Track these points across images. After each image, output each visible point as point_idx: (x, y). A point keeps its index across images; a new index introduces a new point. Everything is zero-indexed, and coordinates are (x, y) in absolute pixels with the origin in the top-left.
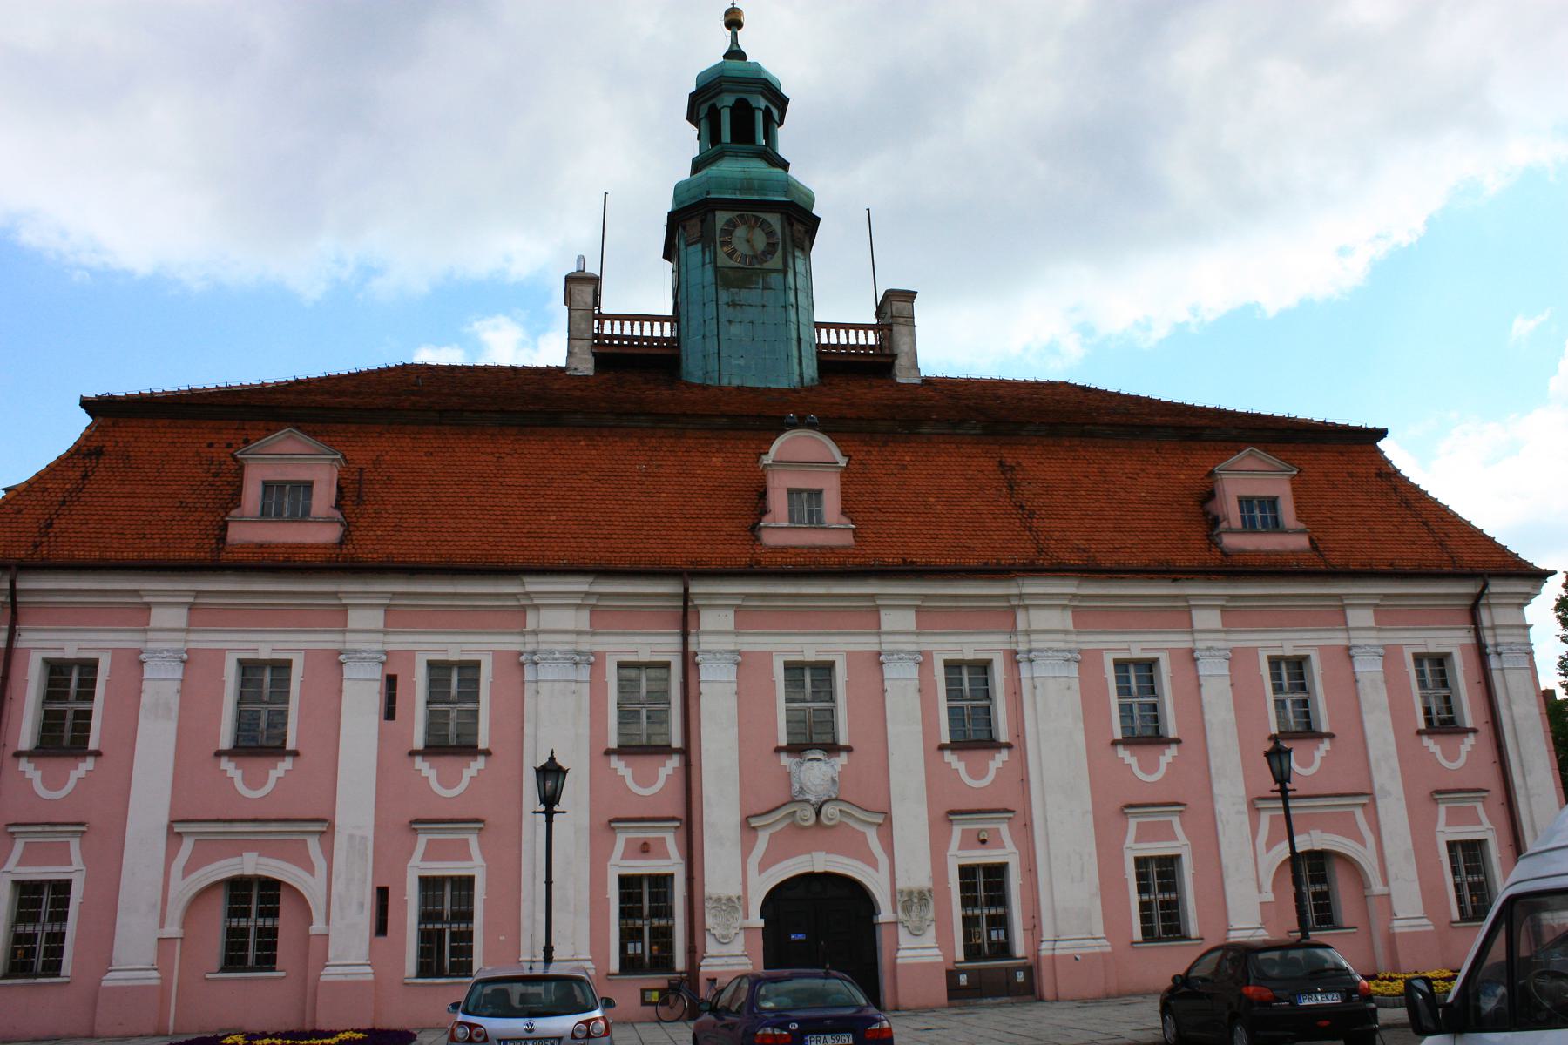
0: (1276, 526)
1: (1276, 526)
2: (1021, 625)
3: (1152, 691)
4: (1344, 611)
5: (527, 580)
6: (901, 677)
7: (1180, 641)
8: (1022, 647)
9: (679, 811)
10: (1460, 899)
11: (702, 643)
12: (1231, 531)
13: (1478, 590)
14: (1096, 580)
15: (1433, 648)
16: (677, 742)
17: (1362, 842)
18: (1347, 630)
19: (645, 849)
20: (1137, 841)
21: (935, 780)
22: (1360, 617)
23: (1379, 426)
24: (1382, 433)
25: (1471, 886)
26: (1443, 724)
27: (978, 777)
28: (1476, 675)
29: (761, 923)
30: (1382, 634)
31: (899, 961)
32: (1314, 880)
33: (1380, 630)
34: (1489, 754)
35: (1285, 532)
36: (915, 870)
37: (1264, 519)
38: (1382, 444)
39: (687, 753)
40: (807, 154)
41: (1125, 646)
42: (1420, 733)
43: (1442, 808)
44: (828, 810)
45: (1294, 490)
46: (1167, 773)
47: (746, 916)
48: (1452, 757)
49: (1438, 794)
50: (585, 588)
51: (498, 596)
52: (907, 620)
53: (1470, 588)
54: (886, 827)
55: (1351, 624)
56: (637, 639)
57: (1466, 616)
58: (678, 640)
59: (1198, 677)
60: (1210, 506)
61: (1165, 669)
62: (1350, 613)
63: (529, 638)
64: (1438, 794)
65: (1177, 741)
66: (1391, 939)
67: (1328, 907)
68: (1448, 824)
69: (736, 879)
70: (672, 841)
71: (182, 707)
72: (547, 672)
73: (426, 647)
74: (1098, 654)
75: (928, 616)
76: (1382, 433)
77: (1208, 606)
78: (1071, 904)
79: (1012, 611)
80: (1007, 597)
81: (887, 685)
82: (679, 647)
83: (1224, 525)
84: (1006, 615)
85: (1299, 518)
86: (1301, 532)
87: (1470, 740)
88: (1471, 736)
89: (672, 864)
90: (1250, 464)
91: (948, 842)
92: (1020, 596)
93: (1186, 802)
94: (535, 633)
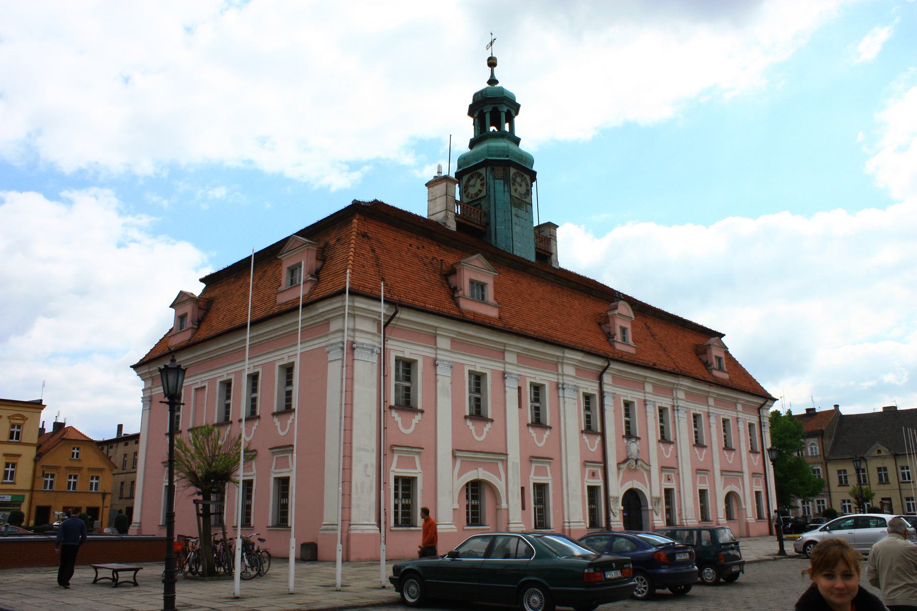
0: (482, 299)
1: (482, 299)
2: (560, 371)
4: (436, 337)
5: (566, 351)
7: (499, 367)
8: (561, 381)
10: (396, 514)
11: (606, 388)
13: (392, 314)
15: (407, 355)
16: (599, 430)
17: (500, 478)
18: (436, 349)
19: (593, 474)
20: (397, 467)
21: (524, 442)
25: (404, 506)
27: (541, 440)
29: (622, 508)
30: (453, 355)
31: (439, 531)
32: (406, 496)
33: (452, 352)
35: (487, 304)
40: (530, 132)
41: (402, 349)
43: (534, 465)
44: (639, 463)
45: (495, 283)
46: (414, 431)
48: (480, 434)
49: (533, 459)
50: (580, 358)
51: (663, 381)
53: (600, 363)
54: (649, 472)
55: (439, 345)
56: (588, 383)
58: (597, 385)
59: (436, 375)
60: (452, 280)
62: (439, 339)
64: (533, 459)
65: (422, 412)
68: (535, 475)
70: (600, 473)
71: (452, 389)
73: (398, 348)
76: (724, 335)
78: (355, 502)
79: (556, 364)
81: (507, 389)
83: (461, 293)
84: (554, 366)
85: (495, 299)
86: (495, 306)
88: (420, 415)
90: (477, 264)
92: (677, 384)
93: (422, 449)
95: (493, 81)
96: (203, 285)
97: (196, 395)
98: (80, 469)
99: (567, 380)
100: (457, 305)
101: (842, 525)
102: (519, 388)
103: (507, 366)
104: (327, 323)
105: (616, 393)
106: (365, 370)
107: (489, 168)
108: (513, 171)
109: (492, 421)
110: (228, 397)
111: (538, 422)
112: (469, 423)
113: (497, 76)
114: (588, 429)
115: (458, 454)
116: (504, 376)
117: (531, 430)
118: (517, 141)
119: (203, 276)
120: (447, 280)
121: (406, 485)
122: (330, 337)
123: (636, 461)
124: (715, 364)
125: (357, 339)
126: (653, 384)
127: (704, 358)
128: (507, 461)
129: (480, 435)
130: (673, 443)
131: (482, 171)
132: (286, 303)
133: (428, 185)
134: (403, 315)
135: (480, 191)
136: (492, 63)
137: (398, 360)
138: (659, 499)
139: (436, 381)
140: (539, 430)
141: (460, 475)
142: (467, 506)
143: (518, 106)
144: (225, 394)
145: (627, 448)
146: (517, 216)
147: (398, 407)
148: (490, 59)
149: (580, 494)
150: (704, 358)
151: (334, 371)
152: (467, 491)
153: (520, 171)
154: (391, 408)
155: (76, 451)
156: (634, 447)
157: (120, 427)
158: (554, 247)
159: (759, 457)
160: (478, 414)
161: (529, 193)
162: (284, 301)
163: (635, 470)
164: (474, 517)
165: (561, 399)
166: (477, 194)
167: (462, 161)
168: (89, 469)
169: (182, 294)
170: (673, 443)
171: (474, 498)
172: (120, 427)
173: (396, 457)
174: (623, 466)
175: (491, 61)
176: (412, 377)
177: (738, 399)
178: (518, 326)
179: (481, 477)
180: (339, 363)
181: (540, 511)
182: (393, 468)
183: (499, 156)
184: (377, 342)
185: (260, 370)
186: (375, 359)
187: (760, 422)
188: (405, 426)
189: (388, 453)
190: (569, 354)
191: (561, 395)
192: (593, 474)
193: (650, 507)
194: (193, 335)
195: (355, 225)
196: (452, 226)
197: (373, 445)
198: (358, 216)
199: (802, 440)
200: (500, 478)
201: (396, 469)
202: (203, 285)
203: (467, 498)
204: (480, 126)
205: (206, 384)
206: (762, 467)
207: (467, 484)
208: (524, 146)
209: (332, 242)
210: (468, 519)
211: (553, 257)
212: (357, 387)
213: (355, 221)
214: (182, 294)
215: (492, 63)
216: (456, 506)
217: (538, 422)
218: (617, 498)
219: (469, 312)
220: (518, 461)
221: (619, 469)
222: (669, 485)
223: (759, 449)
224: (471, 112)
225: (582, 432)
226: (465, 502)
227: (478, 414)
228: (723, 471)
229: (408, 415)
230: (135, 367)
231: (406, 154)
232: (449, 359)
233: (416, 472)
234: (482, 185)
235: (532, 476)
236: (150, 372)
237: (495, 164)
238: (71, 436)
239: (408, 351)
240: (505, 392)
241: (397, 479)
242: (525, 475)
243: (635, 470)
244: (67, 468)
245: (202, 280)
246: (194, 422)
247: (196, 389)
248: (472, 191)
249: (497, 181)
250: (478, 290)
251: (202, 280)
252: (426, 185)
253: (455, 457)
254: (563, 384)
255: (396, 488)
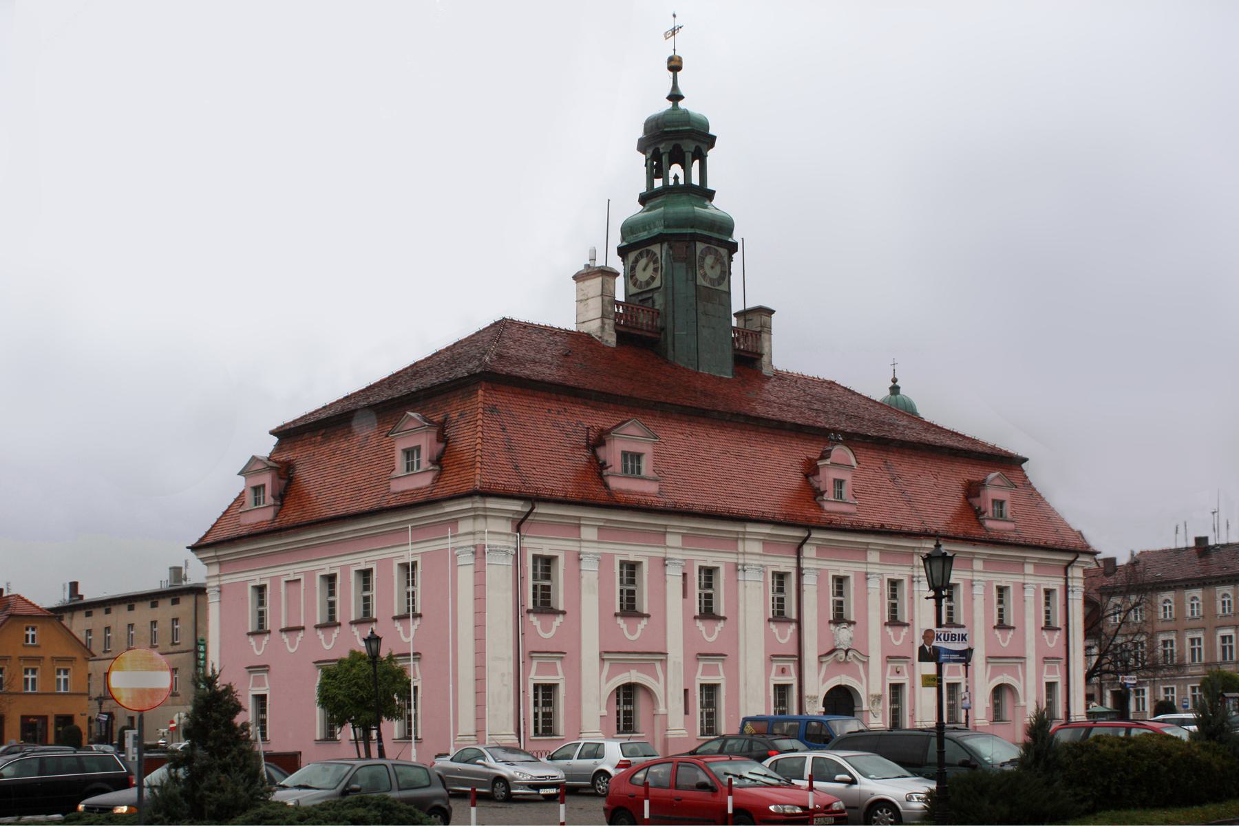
2: (741, 550)
3: (548, 577)
6: (589, 569)
7: (572, 546)
9: (793, 651)
10: (536, 723)
11: (806, 564)
12: (614, 475)
13: (527, 510)
14: (626, 513)
16: (794, 616)
19: (783, 671)
20: (537, 674)
21: (689, 637)
22: (589, 533)
23: (1025, 456)
24: (1025, 460)
25: (544, 714)
26: (1048, 627)
27: (710, 634)
28: (1063, 602)
30: (601, 546)
34: (1063, 641)
36: (876, 689)
37: (633, 467)
38: (1024, 466)
39: (799, 622)
40: (731, 181)
42: (616, 615)
43: (701, 664)
44: (850, 653)
47: (1101, 704)
48: (633, 632)
50: (469, 506)
52: (756, 547)
54: (866, 663)
55: (583, 537)
57: (793, 550)
58: (795, 561)
60: (601, 452)
61: (722, 572)
63: (740, 556)
65: (564, 613)
66: (666, 741)
67: (550, 722)
69: (817, 686)
70: (792, 667)
72: (750, 576)
74: (991, 582)
75: (689, 539)
76: (1025, 460)
77: (591, 522)
80: (738, 533)
82: (795, 565)
87: (1058, 633)
89: (791, 679)
91: (696, 671)
94: (744, 553)
95: (675, 97)
96: (275, 440)
97: (287, 589)
98: (38, 659)
99: (750, 560)
100: (606, 485)
101: (777, 731)
102: (684, 575)
103: (669, 550)
104: (456, 521)
105: (818, 566)
106: (499, 574)
107: (665, 246)
108: (700, 246)
109: (648, 616)
110: (332, 593)
111: (708, 612)
112: (620, 621)
113: (683, 89)
114: (779, 616)
115: (606, 656)
116: (664, 562)
117: (699, 623)
118: (710, 195)
119: (274, 427)
120: (594, 452)
121: (546, 692)
122: (459, 539)
123: (847, 652)
124: (990, 510)
125: (487, 543)
126: (881, 551)
127: (975, 501)
128: (666, 660)
129: (633, 633)
130: (908, 625)
131: (656, 249)
132: (403, 493)
133: (578, 278)
134: (540, 509)
135: (653, 278)
136: (675, 66)
137: (535, 557)
138: (878, 698)
139: (580, 578)
140: (709, 623)
141: (608, 679)
142: (618, 713)
143: (713, 138)
144: (327, 590)
145: (833, 636)
146: (705, 314)
147: (534, 611)
148: (671, 59)
149: (762, 692)
150: (975, 501)
151: (466, 577)
152: (618, 696)
153: (719, 238)
154: (529, 612)
155: (30, 633)
156: (844, 635)
157: (74, 586)
158: (766, 344)
159: (1058, 635)
160: (629, 608)
161: (726, 274)
162: (400, 489)
163: (846, 662)
164: (626, 724)
165: (741, 584)
166: (648, 283)
167: (628, 229)
168: (53, 658)
169: (253, 457)
170: (908, 625)
171: (627, 703)
172: (74, 586)
173: (535, 663)
174: (824, 659)
175: (673, 64)
176: (553, 574)
177: (1025, 558)
178: (686, 499)
179: (633, 680)
180: (471, 569)
181: (710, 715)
182: (532, 675)
183: (682, 227)
184: (510, 543)
185: (374, 566)
186: (510, 561)
187: (1067, 586)
188: (544, 630)
189: (527, 660)
190: (751, 528)
191: (741, 578)
192: (783, 671)
193: (865, 707)
194: (276, 515)
195: (480, 398)
196: (611, 339)
197: (510, 652)
198: (484, 384)
199: (197, 795)
200: (657, 679)
201: (535, 676)
202: (275, 440)
203: (618, 703)
204: (656, 168)
205: (302, 577)
206: (1063, 649)
207: (618, 688)
208: (722, 205)
209: (454, 416)
210: (618, 727)
211: (765, 359)
212: (489, 594)
213: (480, 392)
214: (253, 457)
215: (675, 66)
216: (604, 712)
217: (708, 612)
218: (816, 697)
219: (622, 492)
220: (681, 660)
221: (821, 662)
222: (897, 680)
223: (1058, 621)
224: (642, 146)
225: (769, 620)
226: (614, 708)
227: (629, 608)
228: (990, 658)
229: (547, 618)
230: (194, 548)
231: (543, 259)
232: (596, 551)
233: (557, 677)
234: (655, 270)
235: (699, 675)
236: (217, 557)
237: (679, 235)
238: (21, 609)
239: (546, 547)
240: (666, 581)
241: (536, 687)
242: (689, 674)
243: (846, 662)
244: (20, 658)
245: (273, 433)
246: (288, 618)
247: (287, 582)
248: (643, 276)
249: (677, 265)
250: (632, 462)
251: (273, 433)
252: (575, 278)
253: (602, 660)
254: (744, 565)
255: (536, 696)
